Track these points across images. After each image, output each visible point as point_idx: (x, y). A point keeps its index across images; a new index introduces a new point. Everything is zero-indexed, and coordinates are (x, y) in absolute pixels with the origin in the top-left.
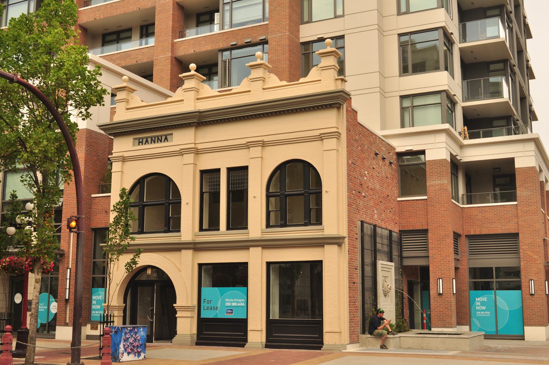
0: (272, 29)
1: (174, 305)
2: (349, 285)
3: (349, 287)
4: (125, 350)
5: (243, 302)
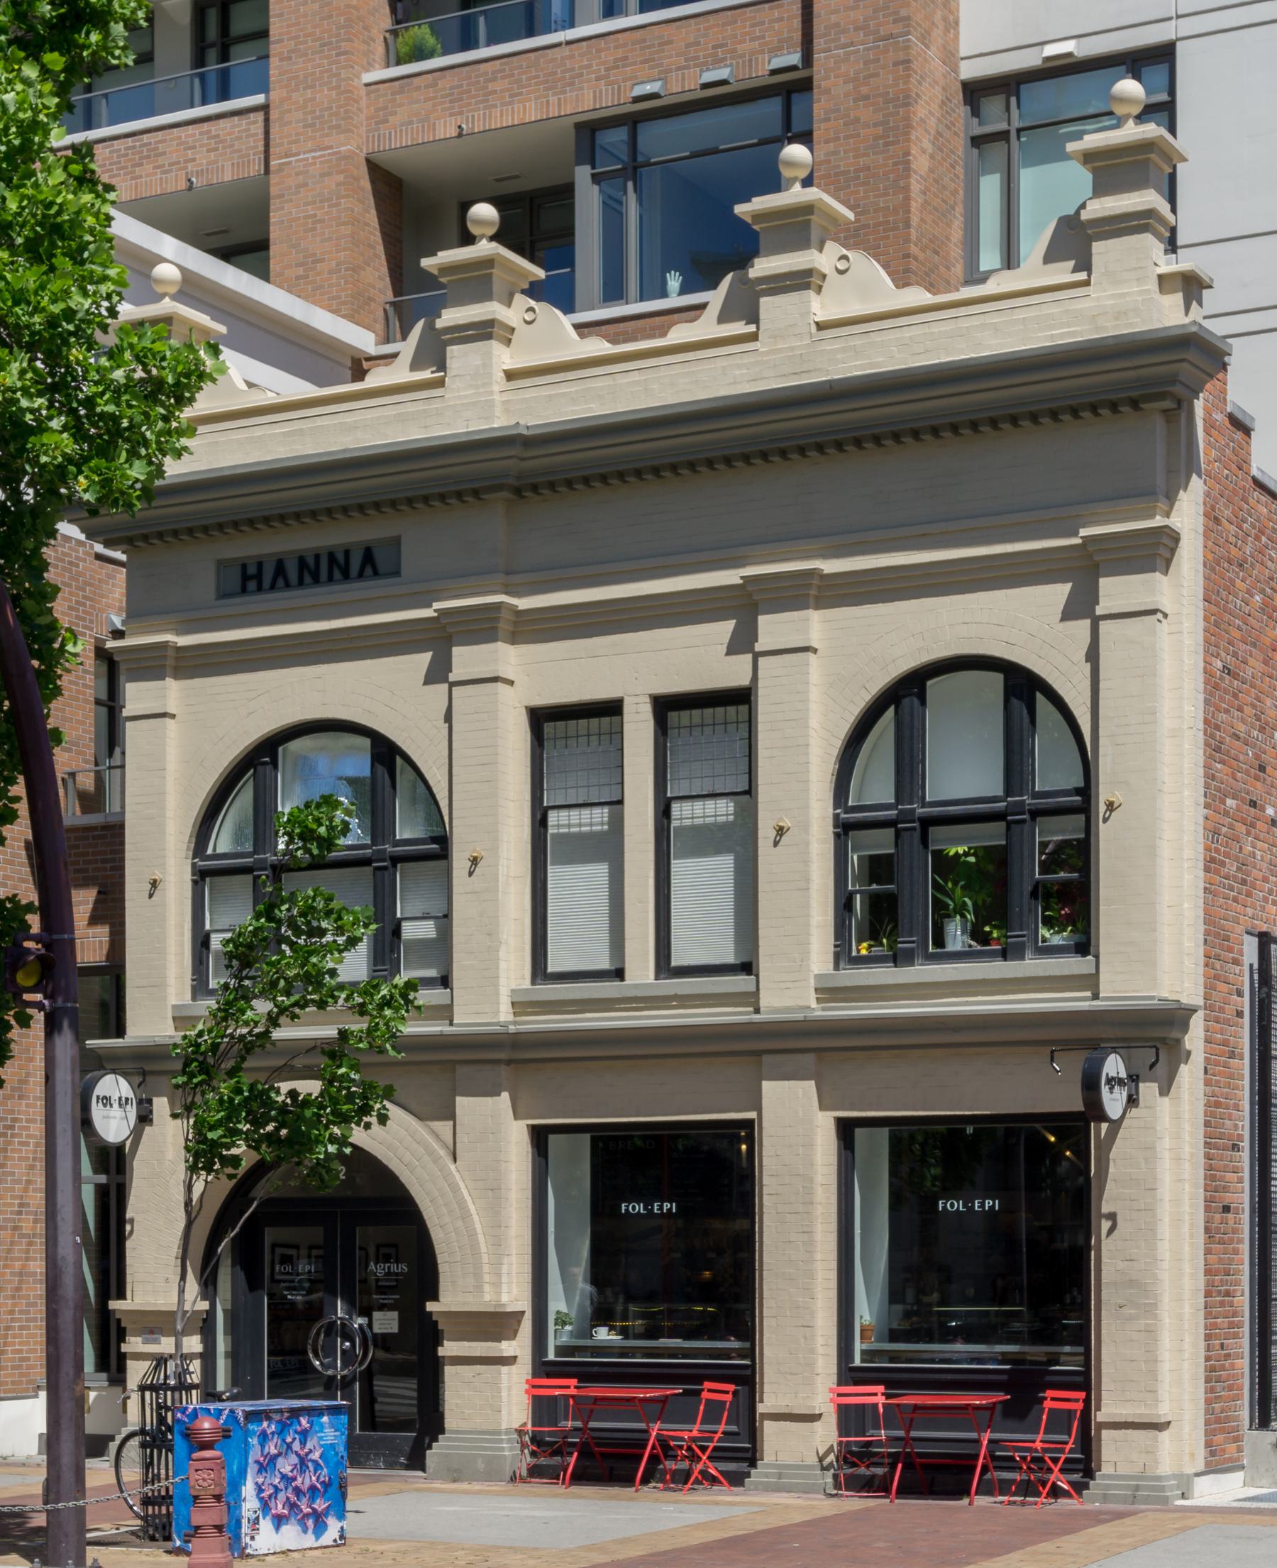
0: (833, 18)
1: (431, 1306)
2: (1208, 1221)
3: (1207, 1230)
4: (265, 1506)
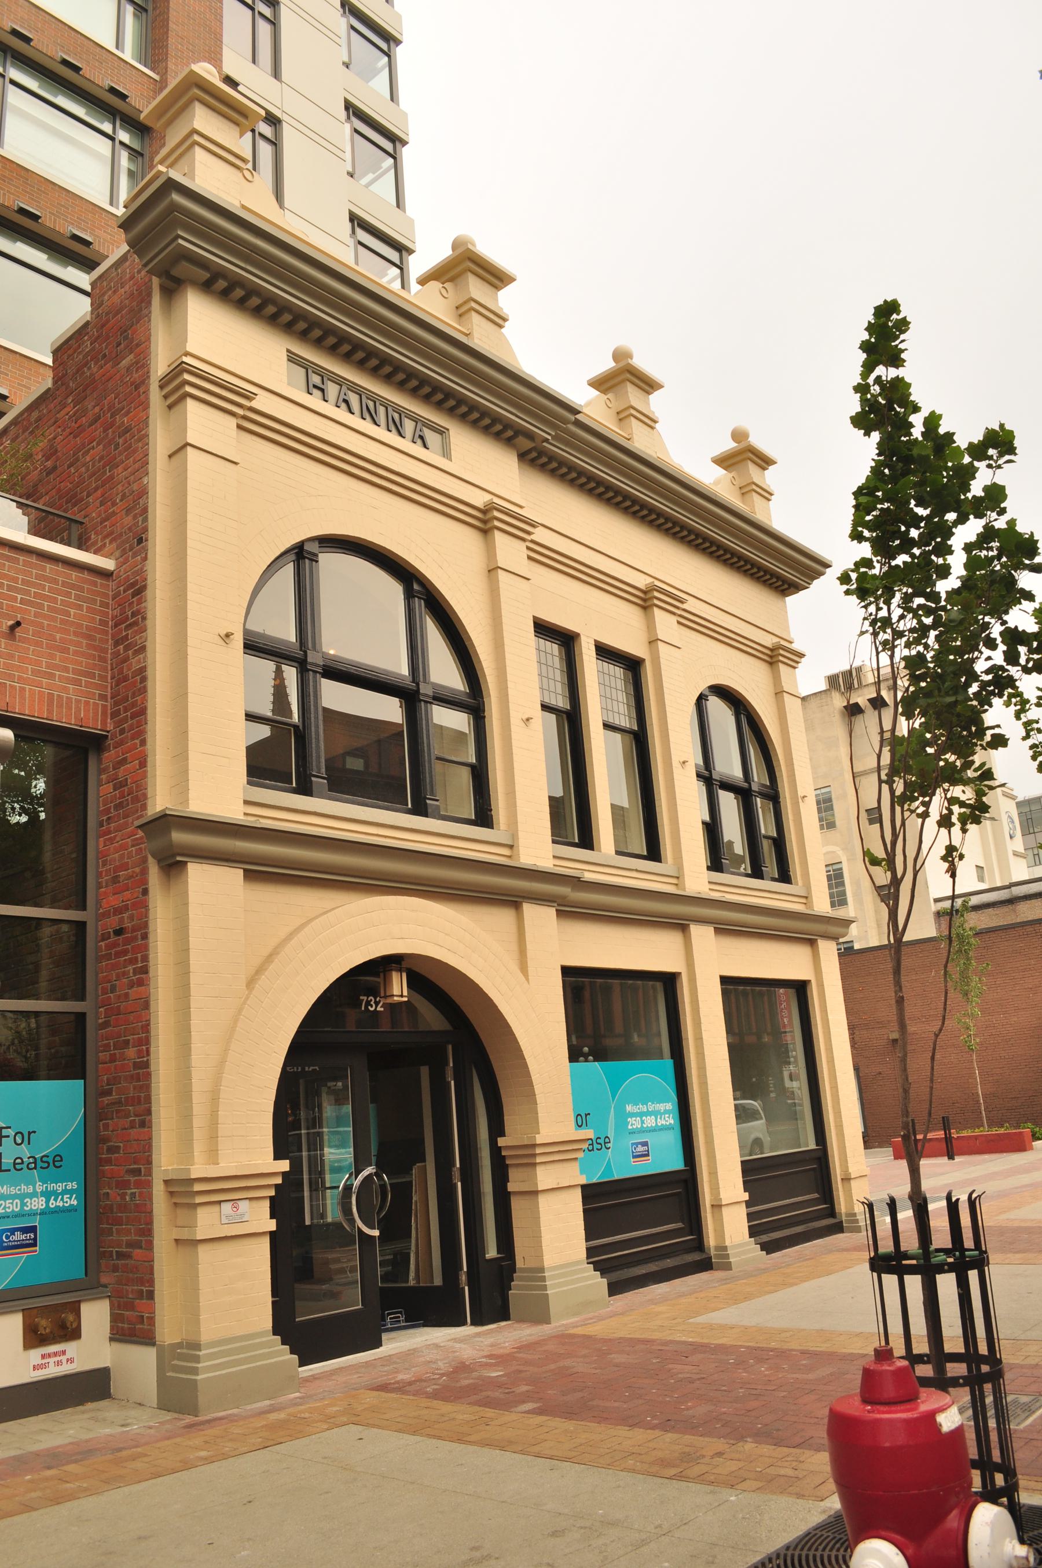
5: (70, 1192)
